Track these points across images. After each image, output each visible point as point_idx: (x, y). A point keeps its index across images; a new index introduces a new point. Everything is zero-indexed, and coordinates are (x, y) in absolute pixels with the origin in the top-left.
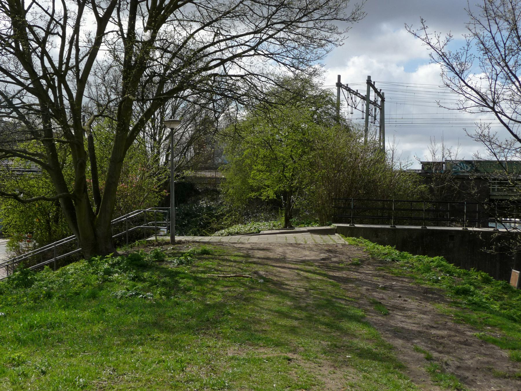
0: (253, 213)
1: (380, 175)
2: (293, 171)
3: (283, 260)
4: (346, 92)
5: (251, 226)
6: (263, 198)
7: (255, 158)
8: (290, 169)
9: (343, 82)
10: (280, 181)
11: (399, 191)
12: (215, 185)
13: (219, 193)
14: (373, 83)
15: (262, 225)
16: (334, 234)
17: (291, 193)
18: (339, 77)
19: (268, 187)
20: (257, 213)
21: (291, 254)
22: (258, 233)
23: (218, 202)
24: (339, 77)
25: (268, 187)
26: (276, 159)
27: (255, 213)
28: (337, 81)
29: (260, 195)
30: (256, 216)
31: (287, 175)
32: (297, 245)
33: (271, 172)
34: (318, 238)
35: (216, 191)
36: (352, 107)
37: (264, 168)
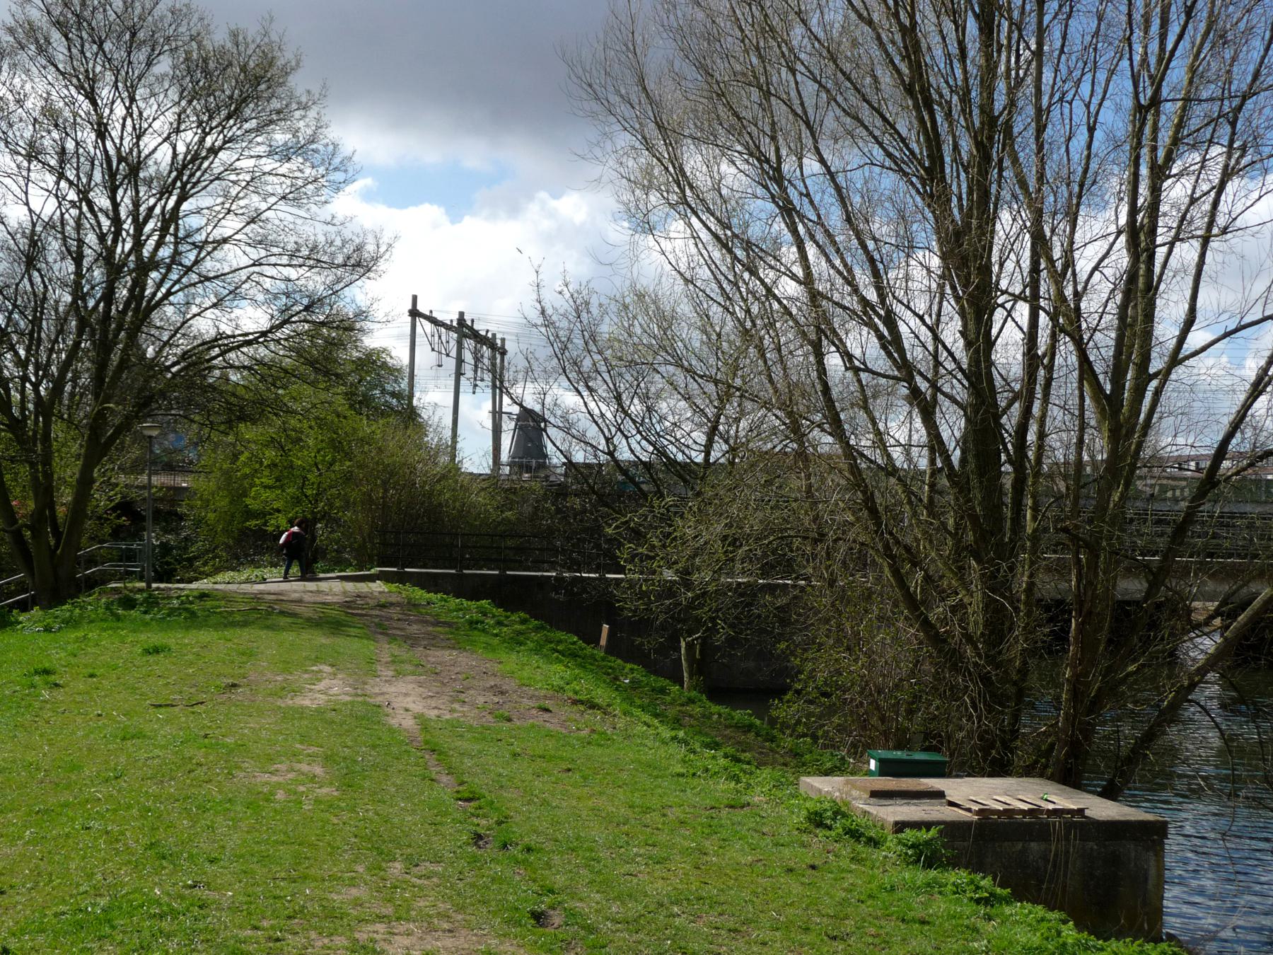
0: (246, 555)
1: (447, 496)
2: (319, 487)
3: (300, 601)
4: (428, 326)
5: (246, 573)
6: (270, 529)
7: (257, 466)
8: (313, 484)
9: (421, 307)
10: (297, 501)
11: (475, 520)
12: (173, 502)
13: (181, 518)
14: (469, 323)
15: (267, 573)
16: (374, 581)
17: (315, 521)
18: (415, 298)
19: (278, 511)
20: (254, 555)
21: (307, 598)
22: (264, 581)
23: (180, 534)
24: (415, 298)
25: (278, 511)
26: (292, 467)
27: (251, 555)
28: (410, 307)
29: (265, 524)
30: (253, 560)
31: (309, 492)
32: (319, 592)
33: (282, 488)
34: (350, 586)
35: (176, 514)
36: (440, 353)
37: (270, 482)
